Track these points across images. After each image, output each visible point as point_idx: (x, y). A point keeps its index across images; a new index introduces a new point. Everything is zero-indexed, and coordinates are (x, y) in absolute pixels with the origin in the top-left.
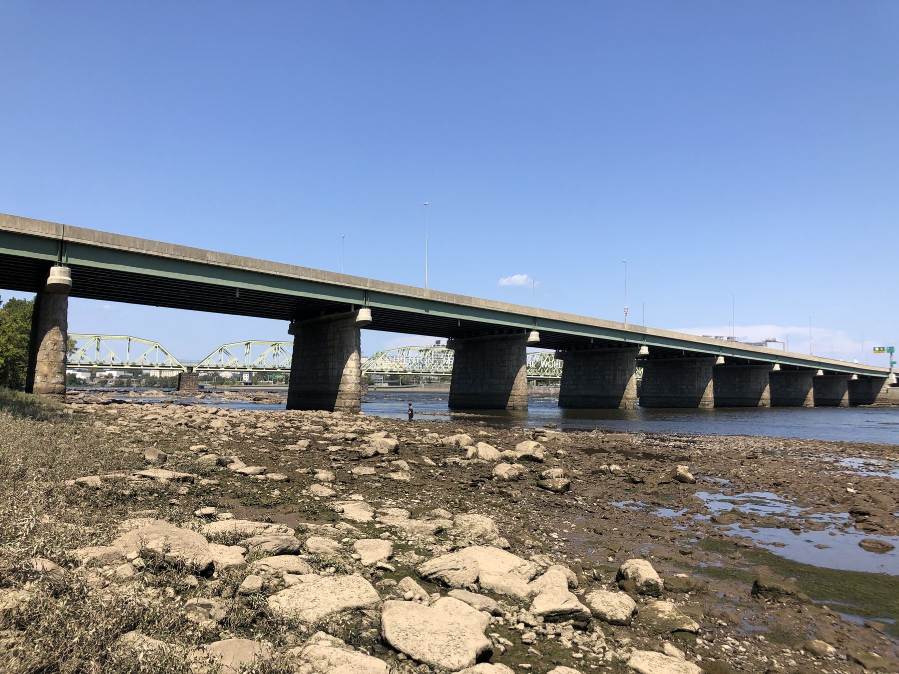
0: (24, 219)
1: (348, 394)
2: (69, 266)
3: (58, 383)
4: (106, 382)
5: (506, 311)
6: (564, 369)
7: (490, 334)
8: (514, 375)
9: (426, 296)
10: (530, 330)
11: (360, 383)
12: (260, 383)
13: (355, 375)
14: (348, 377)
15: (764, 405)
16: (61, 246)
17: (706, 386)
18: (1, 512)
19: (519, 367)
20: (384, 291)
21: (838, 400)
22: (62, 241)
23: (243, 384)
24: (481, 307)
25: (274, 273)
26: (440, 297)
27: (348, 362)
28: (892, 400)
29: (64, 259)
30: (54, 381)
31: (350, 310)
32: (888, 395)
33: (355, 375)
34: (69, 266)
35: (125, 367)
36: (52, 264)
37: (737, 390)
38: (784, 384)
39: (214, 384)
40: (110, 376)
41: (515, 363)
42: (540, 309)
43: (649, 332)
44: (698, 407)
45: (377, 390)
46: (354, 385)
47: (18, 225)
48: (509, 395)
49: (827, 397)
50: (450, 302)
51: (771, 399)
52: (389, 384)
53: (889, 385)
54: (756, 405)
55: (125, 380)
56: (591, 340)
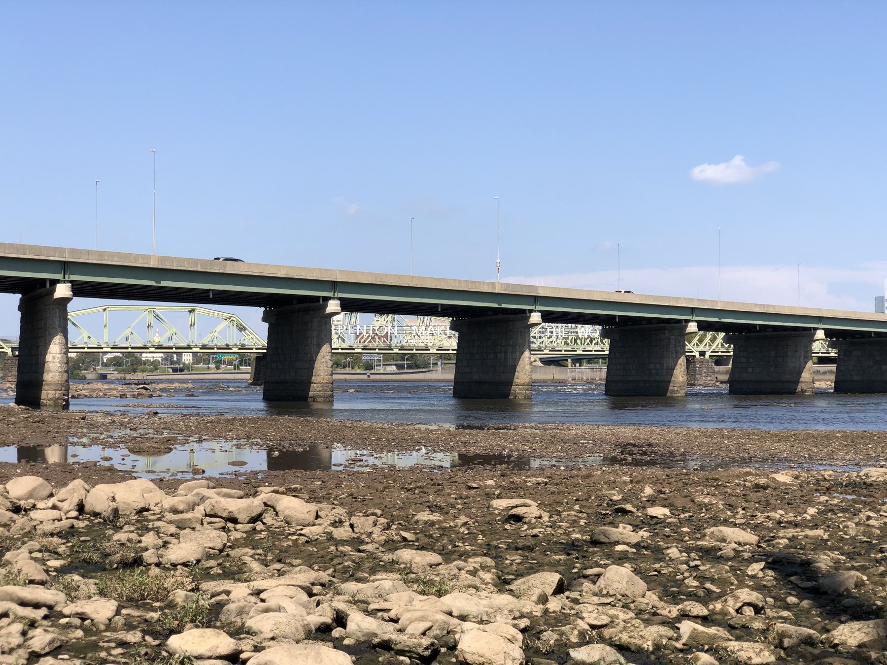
1: (51, 384)
5: (283, 276)
7: (647, 324)
8: (314, 358)
9: (153, 264)
10: (687, 321)
12: (197, 369)
13: (59, 362)
14: (51, 364)
15: (803, 391)
17: (676, 365)
19: (319, 347)
20: (90, 261)
23: (170, 370)
24: (243, 273)
26: (175, 264)
27: (51, 346)
29: (67, 276)
31: (46, 286)
33: (59, 362)
37: (772, 369)
39: (123, 371)
41: (315, 341)
42: (341, 271)
44: (666, 396)
46: (57, 374)
47: (719, 305)
50: (192, 269)
52: (401, 367)
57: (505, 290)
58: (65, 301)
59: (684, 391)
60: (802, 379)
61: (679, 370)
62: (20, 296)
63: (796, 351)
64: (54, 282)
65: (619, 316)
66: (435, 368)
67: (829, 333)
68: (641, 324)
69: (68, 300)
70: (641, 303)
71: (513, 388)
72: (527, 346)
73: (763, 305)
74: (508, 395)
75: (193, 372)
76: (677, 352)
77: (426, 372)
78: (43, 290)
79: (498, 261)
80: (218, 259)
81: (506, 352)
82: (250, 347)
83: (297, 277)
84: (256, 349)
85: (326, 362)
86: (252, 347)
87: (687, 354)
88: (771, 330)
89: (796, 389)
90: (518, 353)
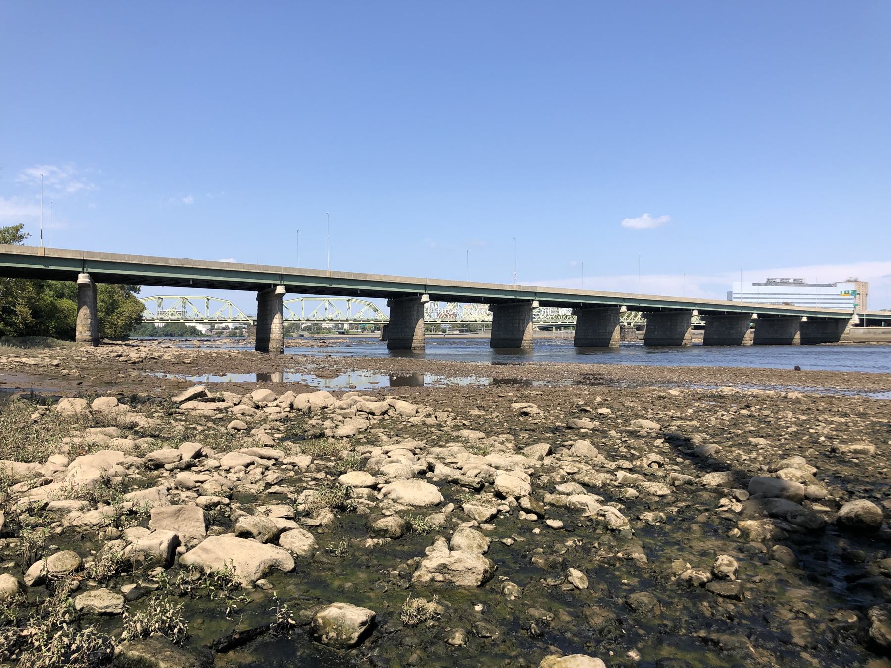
0: (62, 250)
2: (88, 273)
3: (87, 336)
4: (222, 333)
6: (494, 316)
9: (40, 254)
11: (283, 333)
16: (83, 263)
19: (418, 320)
21: (606, 339)
22: (84, 260)
25: (214, 268)
28: (853, 339)
29: (85, 269)
30: (85, 335)
32: (851, 334)
34: (88, 273)
35: (205, 321)
36: (79, 272)
38: (728, 326)
40: (226, 328)
43: (539, 291)
45: (446, 336)
48: (413, 340)
49: (784, 337)
51: (801, 339)
52: (461, 331)
53: (852, 325)
54: (680, 345)
55: (237, 331)
62: (257, 292)
64: (276, 285)
67: (700, 312)
69: (283, 295)
76: (614, 323)
78: (269, 289)
81: (519, 323)
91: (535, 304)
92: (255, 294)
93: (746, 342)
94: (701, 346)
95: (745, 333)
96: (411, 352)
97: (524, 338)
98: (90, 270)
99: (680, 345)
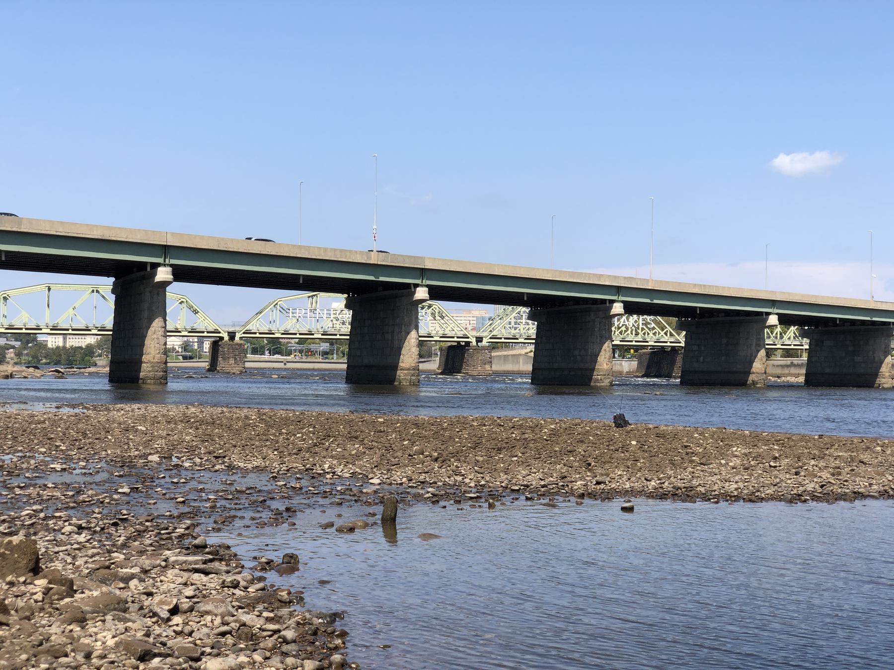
5: (96, 237)
17: (600, 351)
18: (1, 474)
19: (150, 321)
21: (586, 370)
23: (181, 358)
26: (22, 227)
29: (167, 261)
31: (146, 270)
42: (173, 234)
43: (429, 265)
44: (589, 385)
47: (650, 284)
56: (836, 321)
57: (383, 261)
58: (165, 284)
59: (609, 380)
60: (753, 370)
61: (603, 357)
62: (113, 279)
63: (748, 338)
64: (155, 266)
65: (527, 294)
66: (435, 359)
68: (718, 316)
70: (554, 279)
71: (399, 372)
72: (413, 326)
73: (704, 286)
74: (394, 381)
75: (200, 360)
76: (601, 337)
77: (425, 362)
78: (142, 273)
79: (375, 227)
80: (250, 239)
81: (393, 332)
82: (201, 330)
83: (115, 239)
84: (300, 334)
85: (158, 338)
86: (203, 330)
87: (767, 347)
88: (849, 324)
89: (747, 381)
90: (403, 333)
91: (421, 293)
92: (106, 283)
93: (883, 380)
94: (802, 386)
95: (881, 362)
96: (139, 388)
97: (401, 364)
98: (174, 262)
99: (873, 387)
